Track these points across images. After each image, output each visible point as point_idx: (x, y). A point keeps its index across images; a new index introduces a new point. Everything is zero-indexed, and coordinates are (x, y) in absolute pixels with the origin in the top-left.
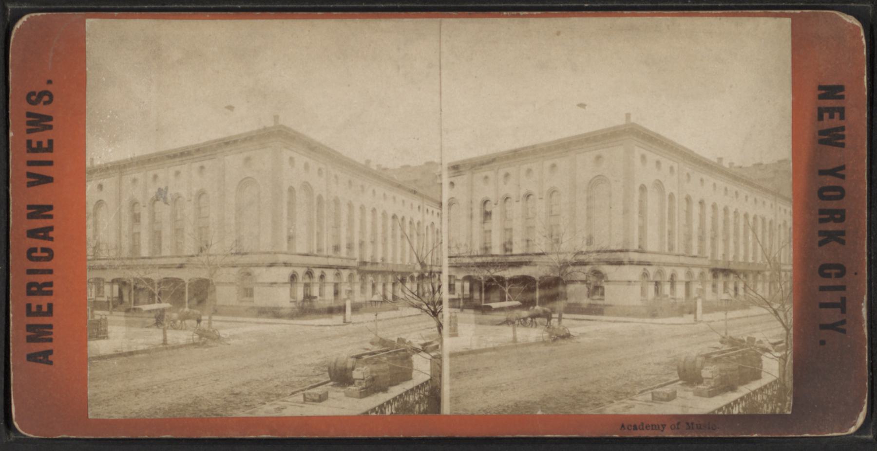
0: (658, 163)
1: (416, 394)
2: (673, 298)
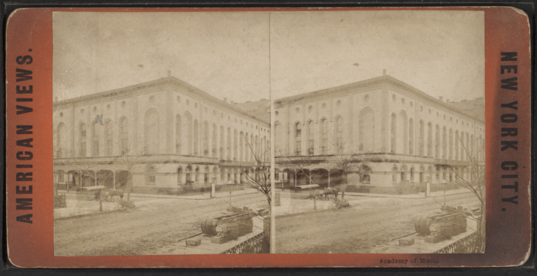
0: (403, 100)
1: (255, 241)
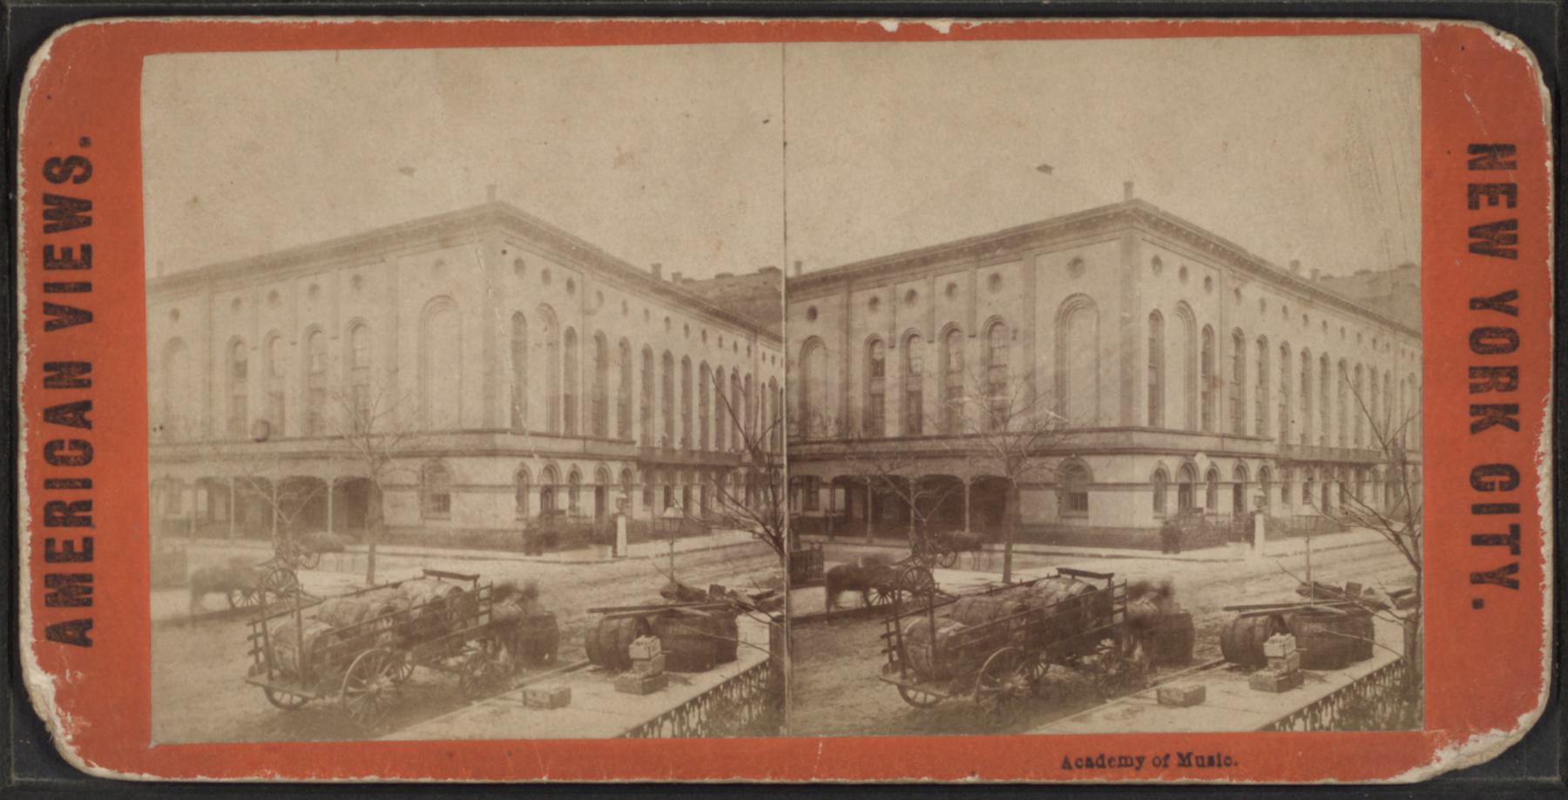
2: (575, 517)
